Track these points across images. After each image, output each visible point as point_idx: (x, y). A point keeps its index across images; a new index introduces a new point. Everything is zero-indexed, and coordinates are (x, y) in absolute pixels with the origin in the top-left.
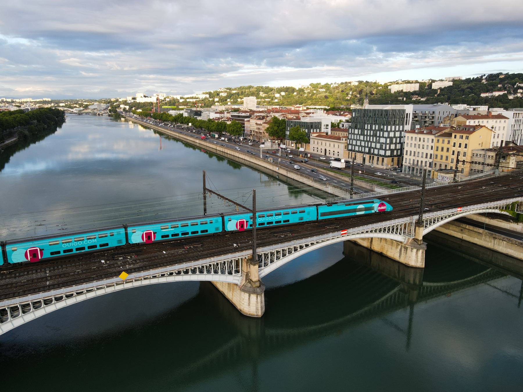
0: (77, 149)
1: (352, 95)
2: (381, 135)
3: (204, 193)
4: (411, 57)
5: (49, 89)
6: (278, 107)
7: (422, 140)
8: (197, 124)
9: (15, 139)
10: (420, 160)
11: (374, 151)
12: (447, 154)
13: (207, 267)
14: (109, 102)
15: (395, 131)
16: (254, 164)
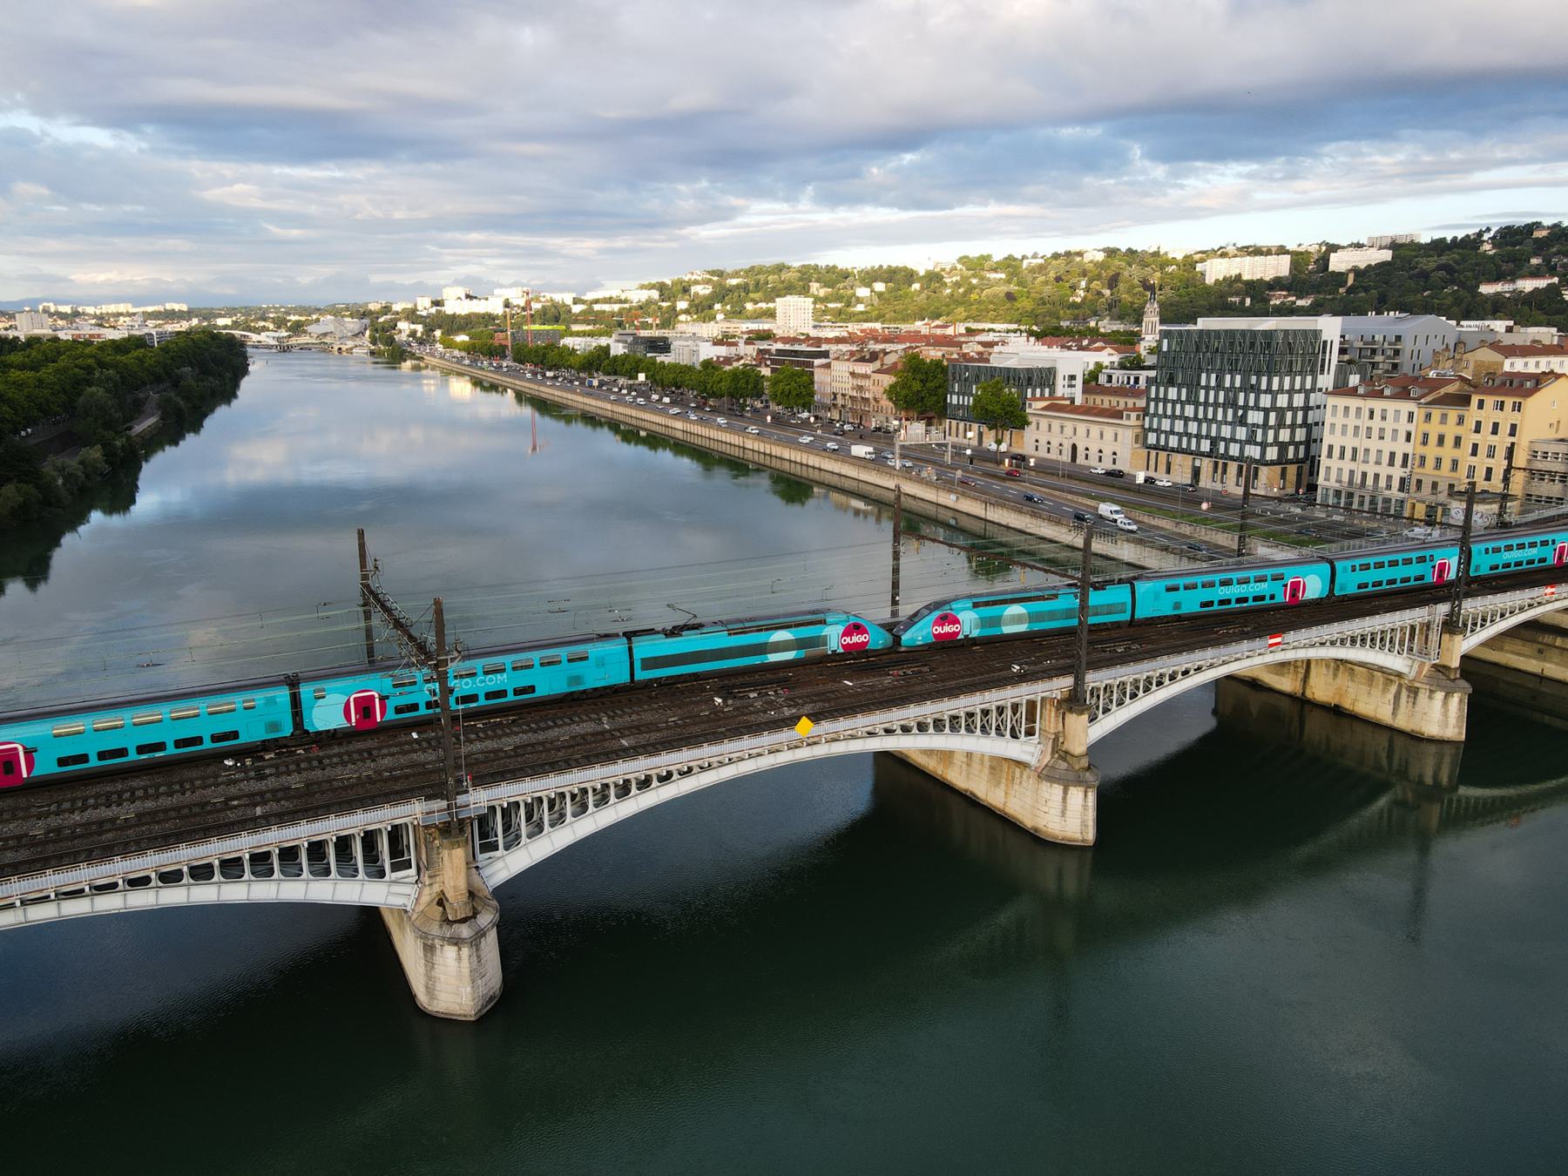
0: (241, 451)
1: (1087, 290)
2: (1251, 403)
4: (1250, 176)
5: (168, 277)
6: (878, 326)
7: (1377, 415)
10: (1371, 470)
11: (1227, 448)
12: (1456, 453)
13: (573, 797)
15: (1291, 392)
16: (871, 488)
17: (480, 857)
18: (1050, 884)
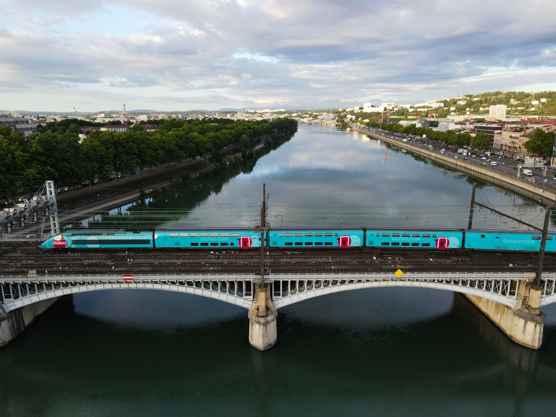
3: (472, 206)
5: (280, 101)
6: (537, 117)
8: (434, 136)
9: (262, 145)
14: (337, 112)
16: (506, 184)
17: (274, 297)
18: (516, 362)
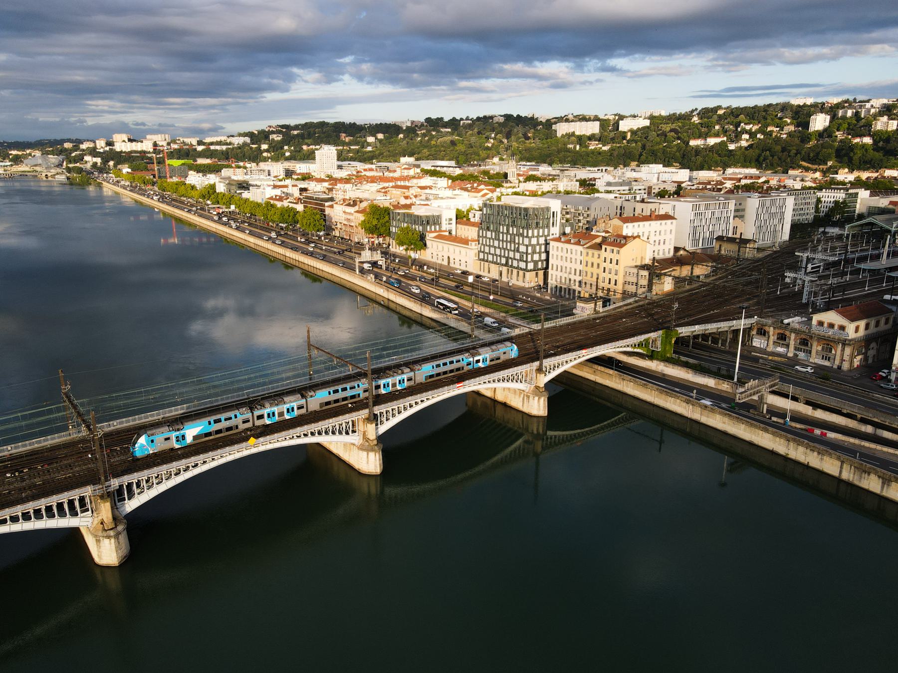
15: (538, 236)
17: (118, 504)
